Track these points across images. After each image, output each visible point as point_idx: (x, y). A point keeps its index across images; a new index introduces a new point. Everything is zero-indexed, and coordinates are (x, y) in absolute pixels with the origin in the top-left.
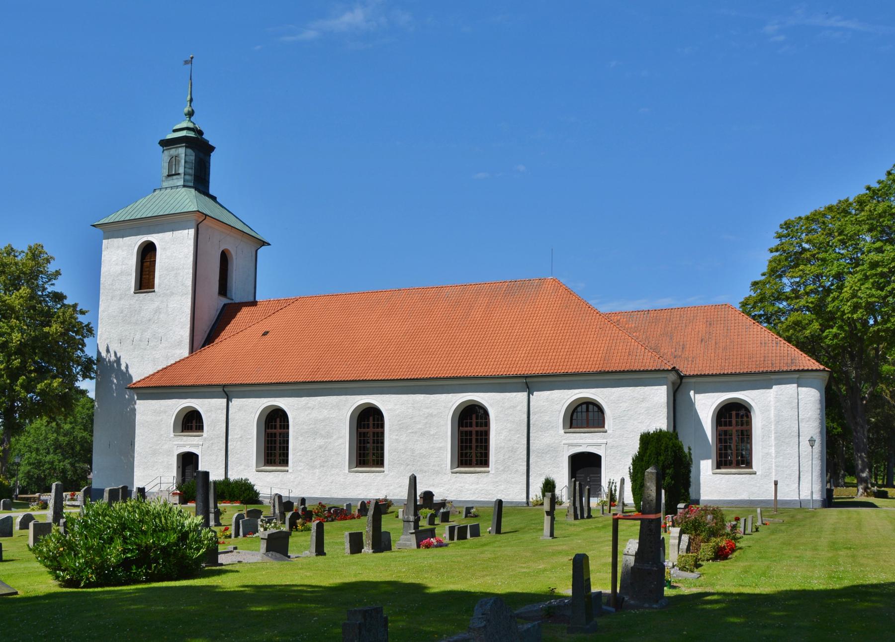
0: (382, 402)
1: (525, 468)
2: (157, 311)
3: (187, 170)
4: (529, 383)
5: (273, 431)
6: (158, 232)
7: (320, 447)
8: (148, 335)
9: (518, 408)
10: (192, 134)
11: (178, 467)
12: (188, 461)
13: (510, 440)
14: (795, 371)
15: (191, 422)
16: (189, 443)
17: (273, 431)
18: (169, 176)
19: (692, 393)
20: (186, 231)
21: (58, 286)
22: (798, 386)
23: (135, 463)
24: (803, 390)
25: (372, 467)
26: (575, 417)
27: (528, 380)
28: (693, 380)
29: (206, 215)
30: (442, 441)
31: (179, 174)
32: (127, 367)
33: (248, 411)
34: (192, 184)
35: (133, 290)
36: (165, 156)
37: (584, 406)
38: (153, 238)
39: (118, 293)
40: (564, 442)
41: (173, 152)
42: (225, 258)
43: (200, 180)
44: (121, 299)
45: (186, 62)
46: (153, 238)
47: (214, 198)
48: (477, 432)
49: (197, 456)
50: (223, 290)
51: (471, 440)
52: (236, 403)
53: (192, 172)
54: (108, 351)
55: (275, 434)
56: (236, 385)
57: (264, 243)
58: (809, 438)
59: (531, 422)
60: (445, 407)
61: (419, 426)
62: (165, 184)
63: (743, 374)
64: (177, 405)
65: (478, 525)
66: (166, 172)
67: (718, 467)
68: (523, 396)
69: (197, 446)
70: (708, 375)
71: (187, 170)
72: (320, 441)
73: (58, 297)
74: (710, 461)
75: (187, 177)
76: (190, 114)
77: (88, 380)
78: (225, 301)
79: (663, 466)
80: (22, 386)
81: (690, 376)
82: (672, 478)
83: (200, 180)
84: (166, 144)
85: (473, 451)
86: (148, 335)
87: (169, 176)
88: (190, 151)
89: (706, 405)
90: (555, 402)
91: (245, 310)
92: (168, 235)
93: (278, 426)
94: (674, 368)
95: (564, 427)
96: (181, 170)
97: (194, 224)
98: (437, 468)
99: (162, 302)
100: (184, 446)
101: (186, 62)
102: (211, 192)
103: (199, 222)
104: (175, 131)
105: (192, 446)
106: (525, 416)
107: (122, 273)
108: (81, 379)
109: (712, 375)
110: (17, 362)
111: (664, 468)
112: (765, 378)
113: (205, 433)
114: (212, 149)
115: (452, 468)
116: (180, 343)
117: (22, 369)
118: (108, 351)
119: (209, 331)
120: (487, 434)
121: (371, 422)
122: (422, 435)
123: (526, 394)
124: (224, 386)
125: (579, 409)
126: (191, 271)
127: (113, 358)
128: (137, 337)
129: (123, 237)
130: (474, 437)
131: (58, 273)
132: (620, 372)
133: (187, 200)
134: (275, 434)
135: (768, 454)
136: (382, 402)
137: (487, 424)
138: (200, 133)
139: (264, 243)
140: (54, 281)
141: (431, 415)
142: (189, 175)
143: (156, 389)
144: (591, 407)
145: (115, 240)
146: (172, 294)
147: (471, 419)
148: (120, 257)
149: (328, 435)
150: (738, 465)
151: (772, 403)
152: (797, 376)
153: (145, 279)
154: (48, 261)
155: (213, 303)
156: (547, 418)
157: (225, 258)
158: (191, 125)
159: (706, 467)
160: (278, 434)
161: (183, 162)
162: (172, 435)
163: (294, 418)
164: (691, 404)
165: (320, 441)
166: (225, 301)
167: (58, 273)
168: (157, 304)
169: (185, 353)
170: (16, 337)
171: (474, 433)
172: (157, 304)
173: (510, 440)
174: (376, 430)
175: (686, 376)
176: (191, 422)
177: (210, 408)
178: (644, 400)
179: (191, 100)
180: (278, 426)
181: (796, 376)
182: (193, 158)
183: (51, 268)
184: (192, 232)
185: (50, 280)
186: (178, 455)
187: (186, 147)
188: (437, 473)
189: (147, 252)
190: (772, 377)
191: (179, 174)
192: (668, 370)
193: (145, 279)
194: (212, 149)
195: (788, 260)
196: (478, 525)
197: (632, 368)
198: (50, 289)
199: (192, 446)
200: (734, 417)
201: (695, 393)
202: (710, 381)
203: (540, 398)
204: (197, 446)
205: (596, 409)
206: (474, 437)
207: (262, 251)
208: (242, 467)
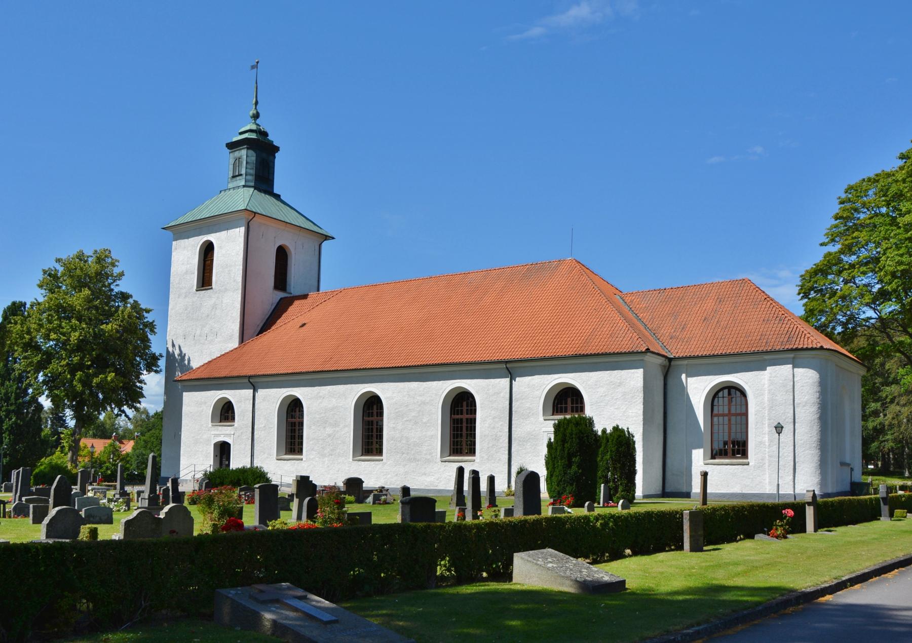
0: (385, 391)
1: (507, 457)
2: (214, 307)
3: (249, 171)
4: (511, 369)
5: (459, 417)
6: (216, 232)
7: (329, 436)
8: (206, 330)
9: (502, 395)
10: (253, 136)
11: (215, 456)
12: (223, 450)
13: (494, 428)
14: (788, 350)
15: (225, 412)
16: (224, 433)
17: (459, 417)
18: (234, 177)
19: (683, 376)
20: (238, 229)
21: (121, 286)
22: (794, 367)
23: (182, 452)
24: (799, 371)
25: (464, 455)
26: (716, 403)
27: (508, 365)
28: (685, 362)
29: (255, 213)
30: (346, 429)
31: (241, 175)
32: (189, 361)
33: (271, 399)
34: (252, 184)
35: (195, 288)
36: (229, 157)
37: (726, 391)
38: (211, 237)
39: (184, 291)
40: (544, 429)
41: (237, 154)
42: (282, 255)
43: (263, 180)
44: (186, 297)
45: (253, 67)
46: (211, 237)
47: (277, 197)
48: (467, 419)
49: (229, 445)
50: (281, 281)
51: (462, 427)
52: (261, 393)
53: (253, 172)
54: (173, 345)
55: (461, 420)
56: (259, 376)
57: (327, 238)
58: (776, 424)
59: (513, 409)
60: (436, 395)
61: (413, 414)
62: (231, 186)
63: (734, 355)
64: (214, 396)
65: (445, 512)
66: (231, 175)
67: (713, 457)
68: (505, 382)
69: (229, 435)
70: (698, 357)
71: (249, 171)
72: (329, 430)
73: (124, 297)
74: (701, 451)
75: (249, 177)
76: (256, 116)
77: (153, 373)
78: (282, 295)
79: (568, 453)
80: (80, 381)
81: (679, 358)
82: (579, 467)
83: (263, 180)
84: (232, 146)
85: (464, 439)
86: (206, 330)
87: (234, 177)
88: (251, 152)
89: (698, 389)
90: (536, 388)
91: (297, 303)
92: (223, 234)
93: (465, 411)
94: (648, 349)
95: (544, 415)
96: (243, 172)
97: (244, 222)
98: (429, 457)
99: (218, 298)
100: (219, 435)
101: (253, 67)
102: (276, 191)
103: (250, 219)
104: (241, 133)
105: (226, 435)
106: (508, 403)
107: (186, 273)
108: (145, 372)
109: (702, 357)
110: (76, 359)
111: (570, 456)
112: (758, 359)
113: (236, 423)
114: (277, 149)
115: (442, 456)
116: (231, 337)
117: (80, 366)
118: (173, 345)
119: (259, 322)
120: (472, 422)
121: (569, 405)
122: (416, 423)
123: (508, 379)
124: (250, 377)
125: (720, 394)
126: (241, 267)
127: (177, 352)
128: (198, 332)
129: (188, 238)
130: (464, 425)
131: (122, 274)
132: (595, 355)
133: (241, 197)
134: (461, 420)
135: (761, 443)
136: (385, 391)
137: (473, 411)
138: (265, 134)
139: (327, 238)
140: (118, 282)
141: (424, 403)
142: (250, 175)
143: (206, 381)
144: (733, 391)
145: (182, 241)
146: (226, 290)
147: (566, 403)
148: (185, 255)
149: (336, 424)
150: (734, 455)
151: (766, 386)
152: (794, 355)
153: (205, 280)
154: (113, 265)
155: (269, 296)
156: (528, 405)
157: (282, 255)
158: (254, 127)
159: (698, 457)
160: (464, 420)
161: (245, 163)
162: (210, 424)
163: (308, 408)
164: (683, 389)
165: (329, 430)
166: (282, 295)
167: (122, 274)
168: (213, 300)
169: (235, 344)
170: (75, 336)
171: (464, 420)
172: (213, 300)
173: (494, 428)
174: (469, 416)
175: (675, 358)
176: (225, 412)
177: (240, 398)
178: (620, 384)
179: (257, 103)
180: (465, 411)
181: (792, 355)
182: (254, 158)
183: (116, 271)
184: (242, 230)
185: (114, 281)
186: (215, 445)
187: (248, 148)
188: (428, 461)
189: (208, 250)
190: (766, 357)
191: (241, 175)
192: (642, 352)
193: (205, 280)
194: (277, 149)
195: (847, 226)
196: (445, 512)
197: (815, 346)
198: (116, 290)
199: (226, 435)
200: (729, 400)
201: (687, 376)
202: (703, 363)
203: (523, 383)
204: (229, 435)
205: (738, 393)
206: (464, 425)
207: (326, 245)
208: (266, 455)
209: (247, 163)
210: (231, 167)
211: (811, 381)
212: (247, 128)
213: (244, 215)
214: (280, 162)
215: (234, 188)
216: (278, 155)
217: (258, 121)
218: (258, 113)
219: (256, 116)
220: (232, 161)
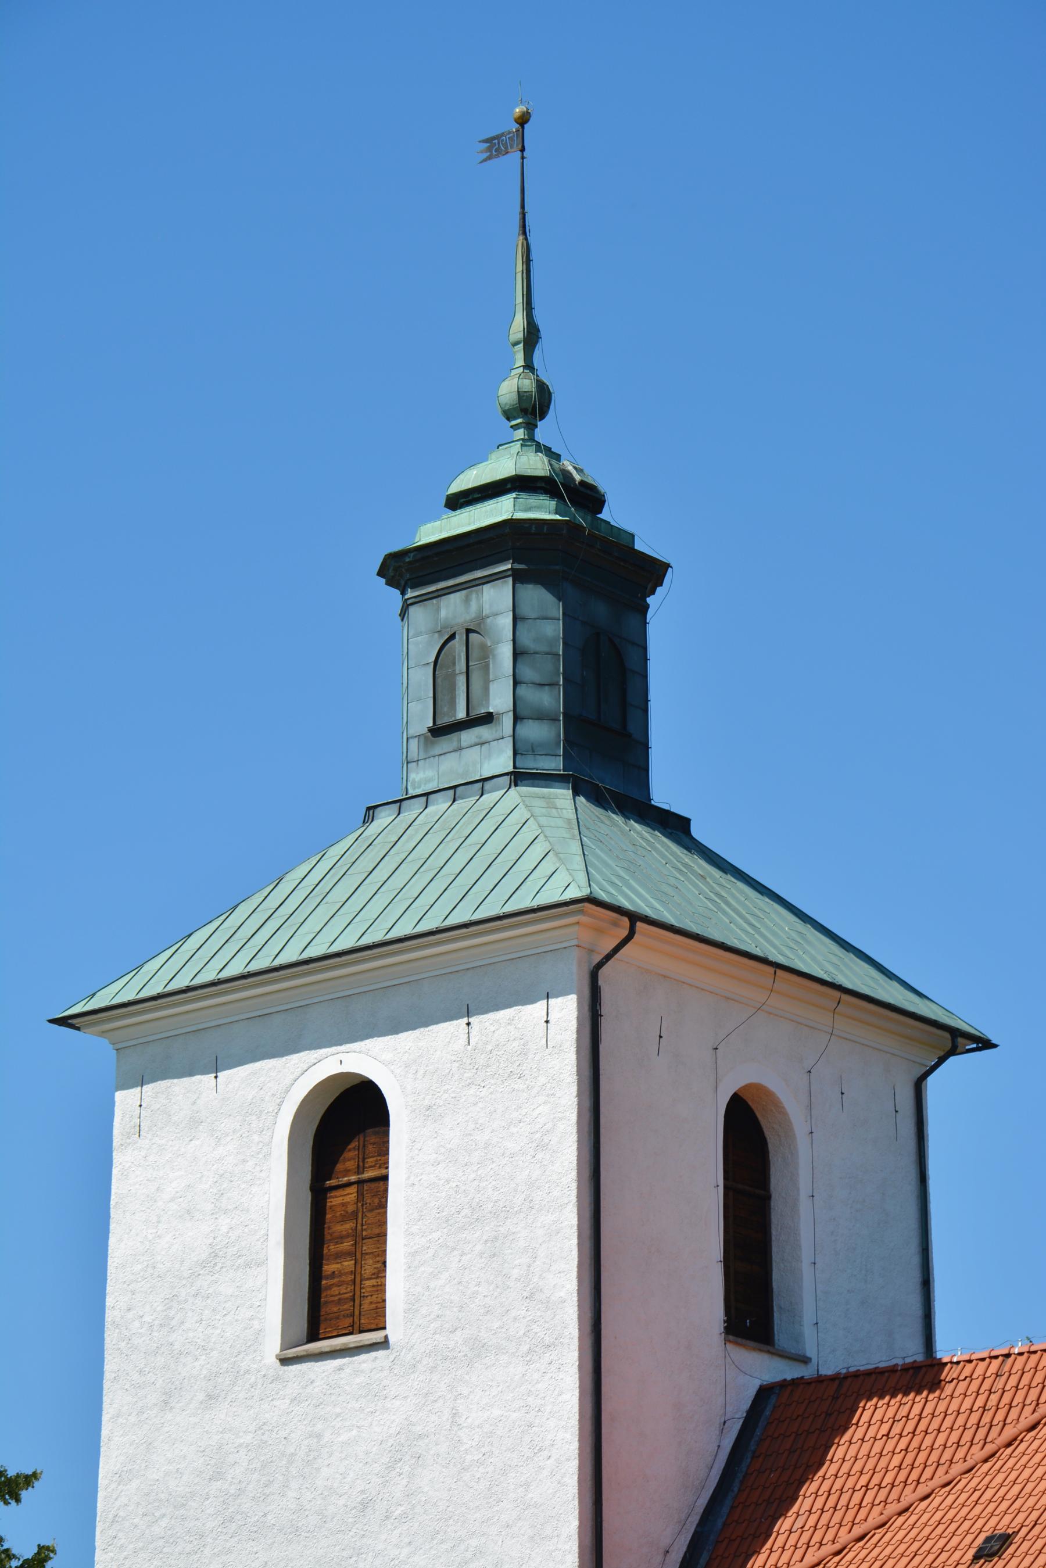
10: (542, 509)
18: (438, 731)
29: (634, 918)
31: (488, 719)
34: (555, 764)
35: (273, 1344)
41: (453, 609)
43: (600, 743)
45: (495, 146)
47: (675, 826)
53: (552, 700)
57: (958, 1041)
62: (422, 778)
75: (534, 731)
76: (533, 408)
78: (760, 1369)
83: (600, 743)
84: (414, 570)
87: (438, 731)
96: (500, 699)
97: (573, 968)
101: (495, 146)
103: (602, 951)
114: (652, 572)
129: (215, 1068)
133: (542, 846)
138: (586, 497)
139: (958, 1041)
142: (541, 716)
145: (179, 1086)
148: (202, 1169)
153: (335, 1294)
155: (697, 1383)
157: (747, 1135)
158: (536, 465)
161: (505, 652)
166: (760, 1369)
179: (532, 337)
182: (554, 630)
184: (566, 1010)
187: (518, 578)
189: (347, 1127)
193: (335, 1294)
194: (652, 572)
209: (517, 654)
210: (422, 678)
211: (492, 591)
212: (503, 465)
213: (568, 932)
214: (669, 623)
215: (454, 791)
216: (661, 606)
217: (544, 432)
218: (543, 390)
219: (533, 408)
220: (422, 646)
